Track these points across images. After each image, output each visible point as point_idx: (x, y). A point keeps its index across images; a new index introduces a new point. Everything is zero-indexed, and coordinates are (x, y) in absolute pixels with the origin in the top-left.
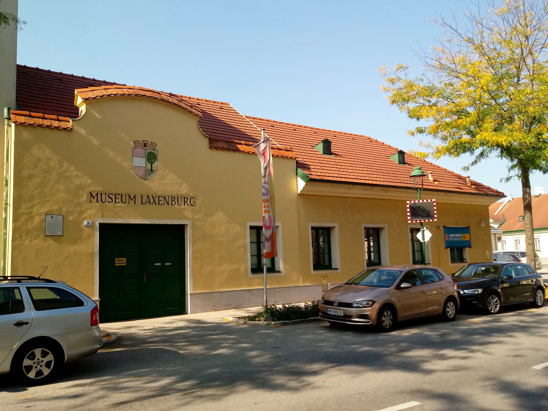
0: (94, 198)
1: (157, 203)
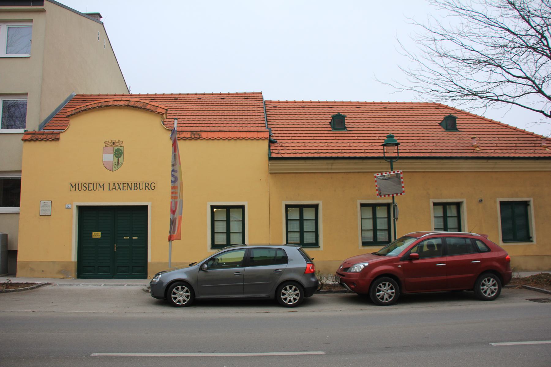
1: (122, 188)
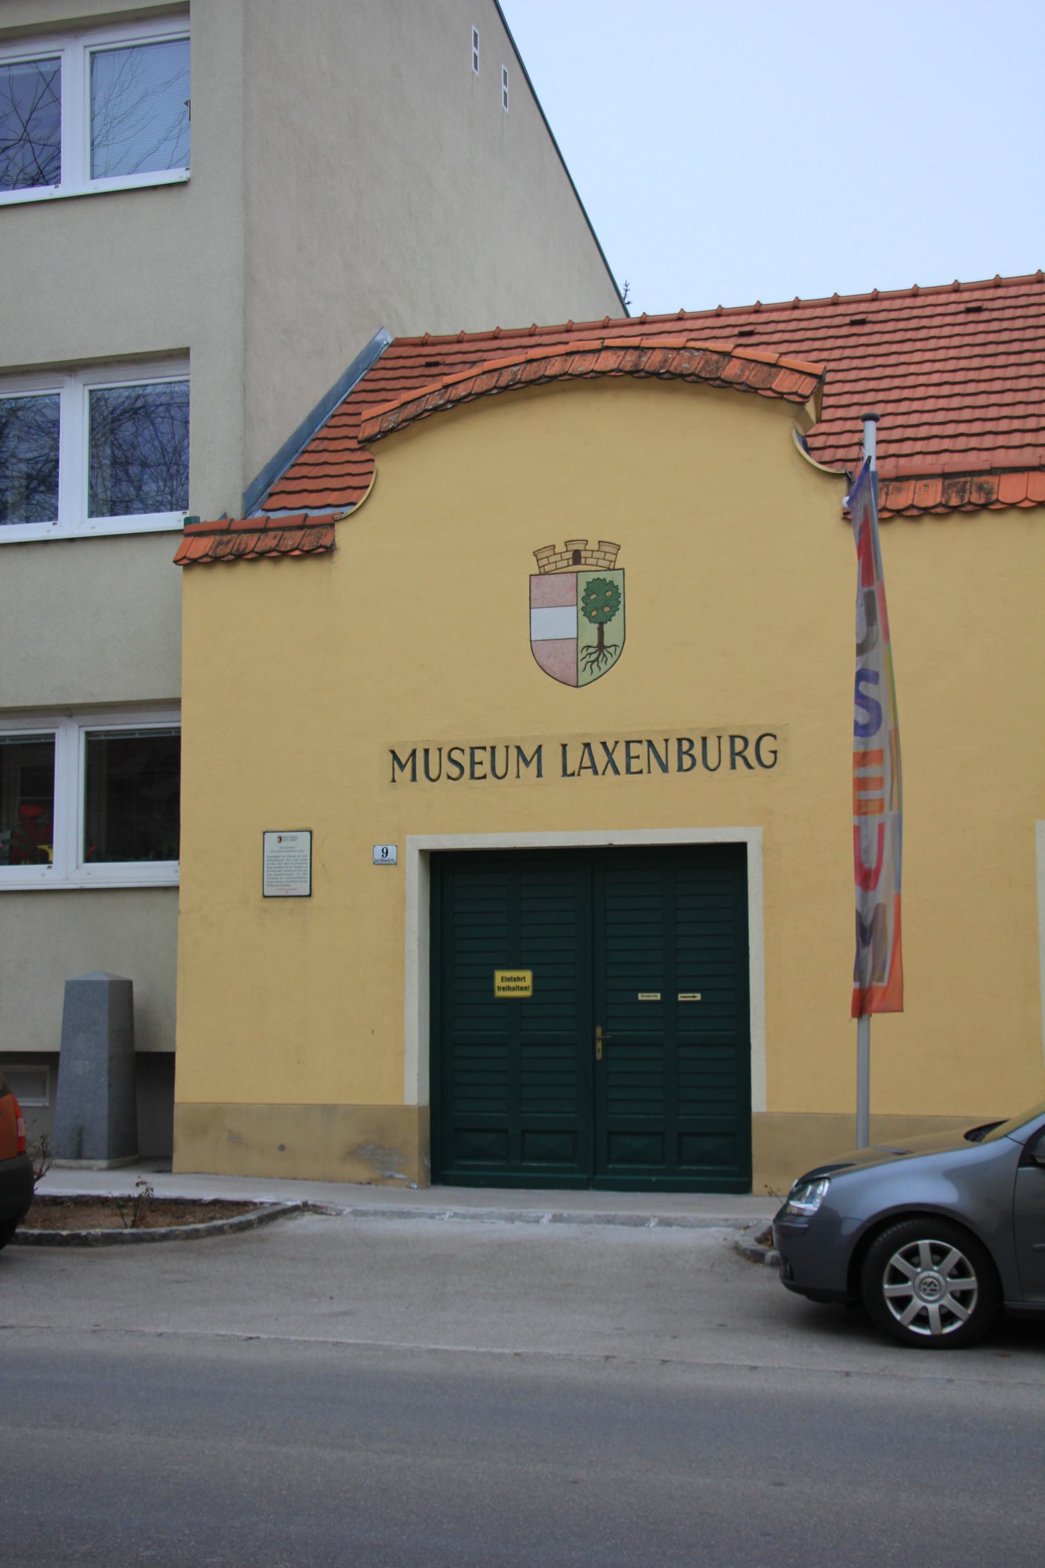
0: (402, 767)
1: (621, 766)
